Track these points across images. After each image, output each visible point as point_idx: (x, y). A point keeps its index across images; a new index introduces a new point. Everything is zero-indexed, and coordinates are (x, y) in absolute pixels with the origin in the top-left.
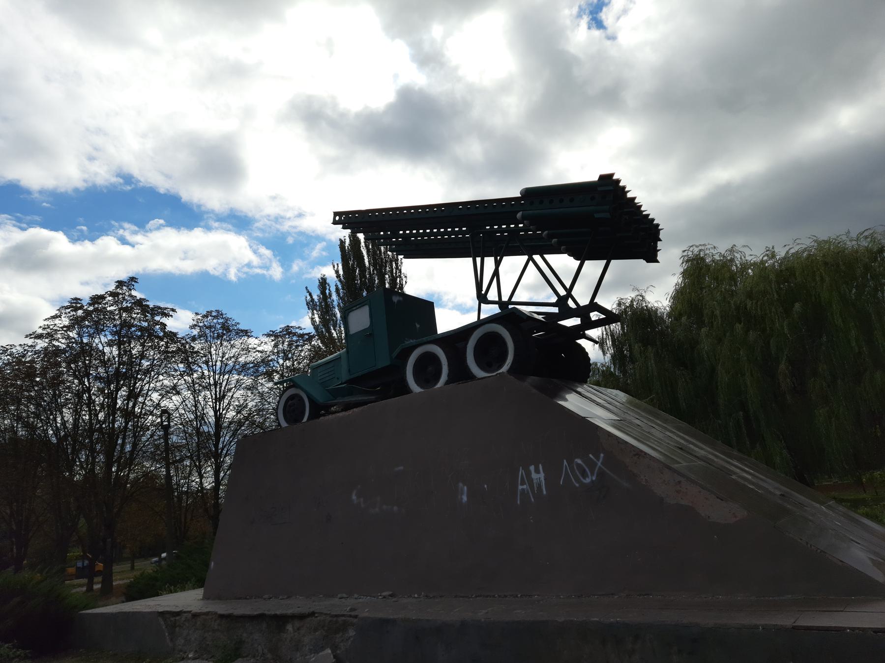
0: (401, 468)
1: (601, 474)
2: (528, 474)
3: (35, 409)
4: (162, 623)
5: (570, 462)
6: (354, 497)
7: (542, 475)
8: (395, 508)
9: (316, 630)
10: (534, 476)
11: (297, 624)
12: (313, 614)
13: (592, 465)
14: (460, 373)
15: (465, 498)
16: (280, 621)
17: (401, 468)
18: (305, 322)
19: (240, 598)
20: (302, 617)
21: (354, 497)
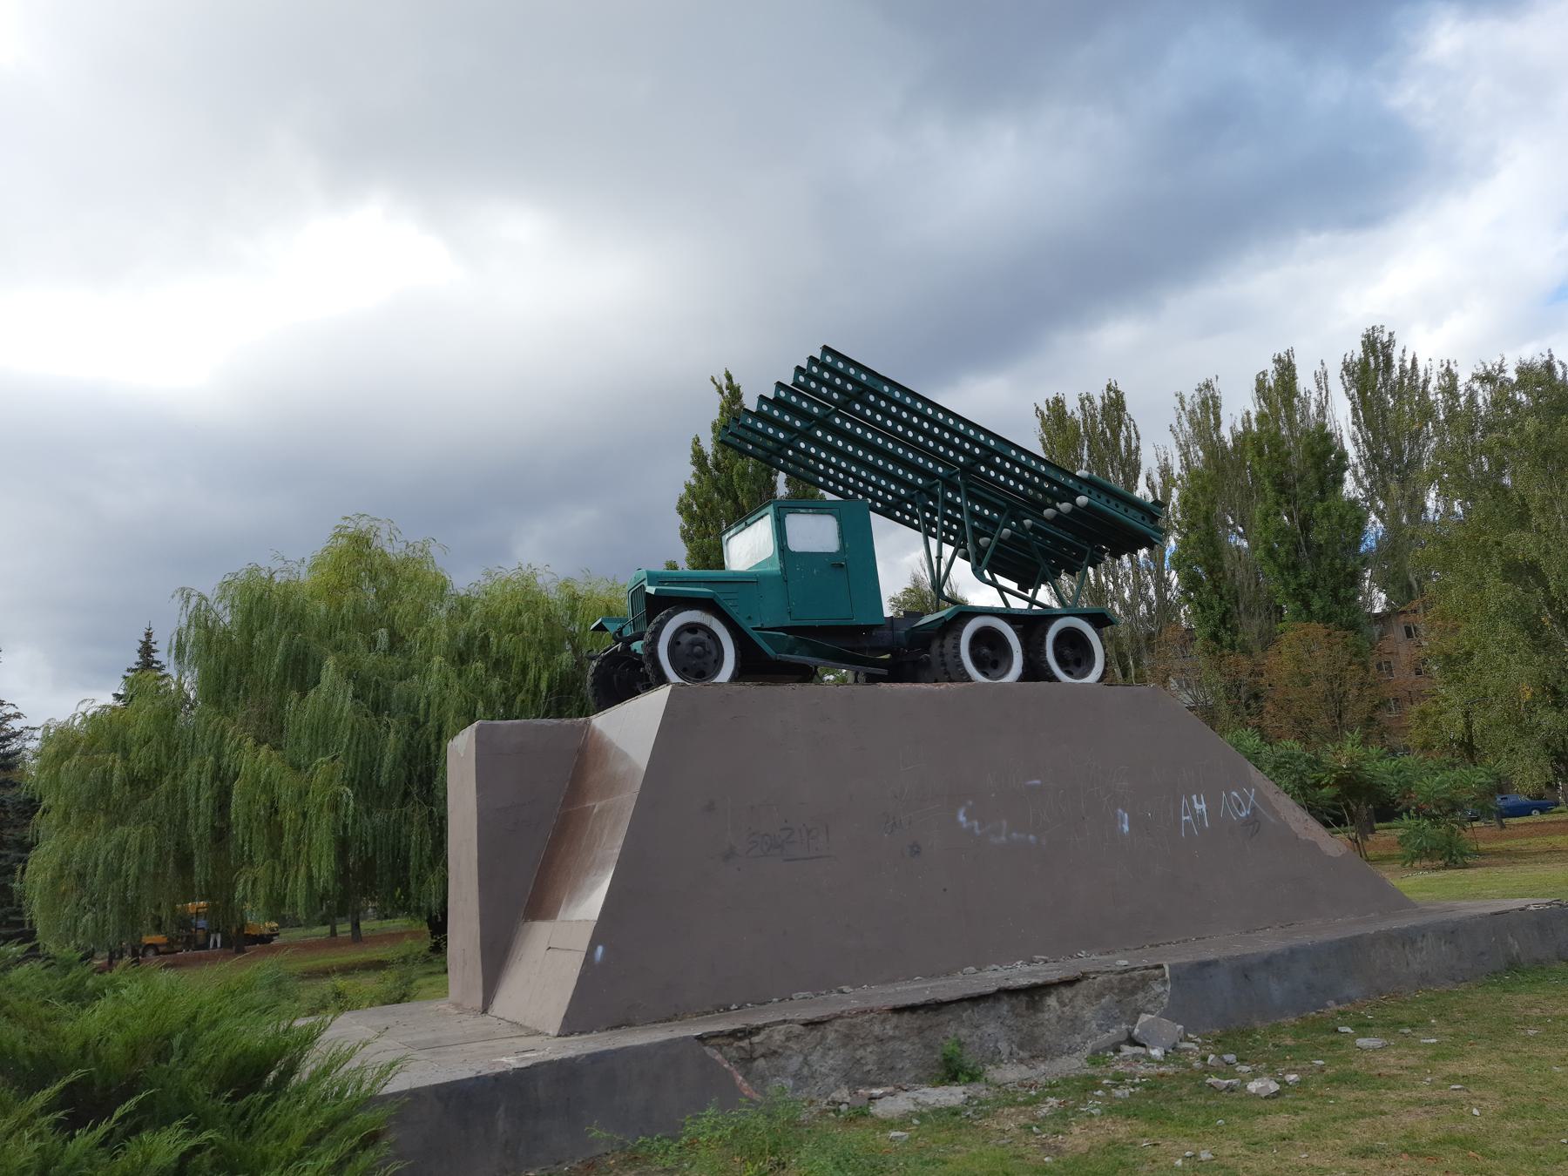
0: (1037, 782)
1: (1253, 808)
2: (1191, 803)
3: (1131, 597)
4: (719, 1057)
5: (1228, 795)
6: (962, 818)
7: (1203, 806)
8: (1031, 837)
9: (1100, 996)
10: (1197, 806)
11: (1067, 993)
12: (1085, 976)
13: (1246, 799)
14: (1035, 671)
15: (1126, 828)
16: (1034, 994)
17: (1037, 782)
18: (693, 482)
19: (618, 1027)
20: (1069, 983)
21: (962, 818)
